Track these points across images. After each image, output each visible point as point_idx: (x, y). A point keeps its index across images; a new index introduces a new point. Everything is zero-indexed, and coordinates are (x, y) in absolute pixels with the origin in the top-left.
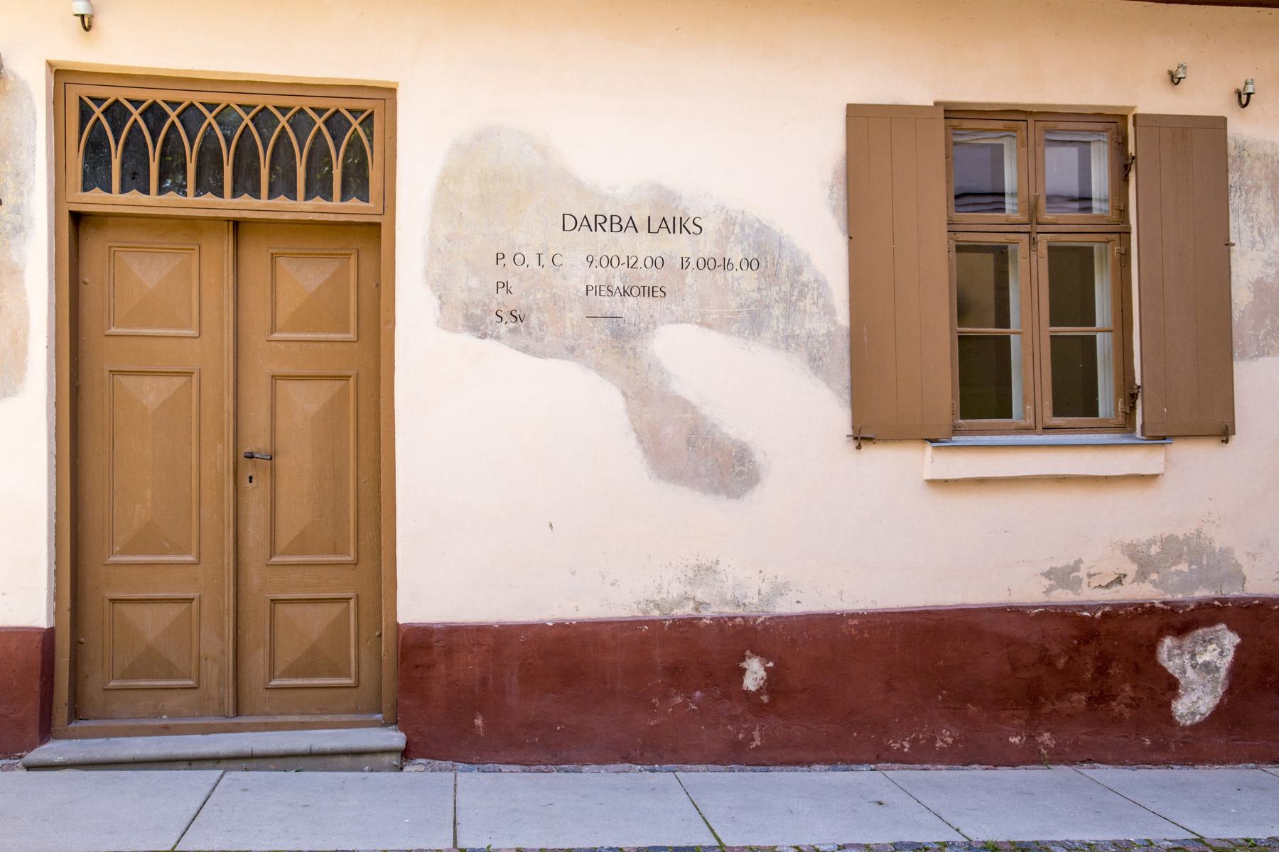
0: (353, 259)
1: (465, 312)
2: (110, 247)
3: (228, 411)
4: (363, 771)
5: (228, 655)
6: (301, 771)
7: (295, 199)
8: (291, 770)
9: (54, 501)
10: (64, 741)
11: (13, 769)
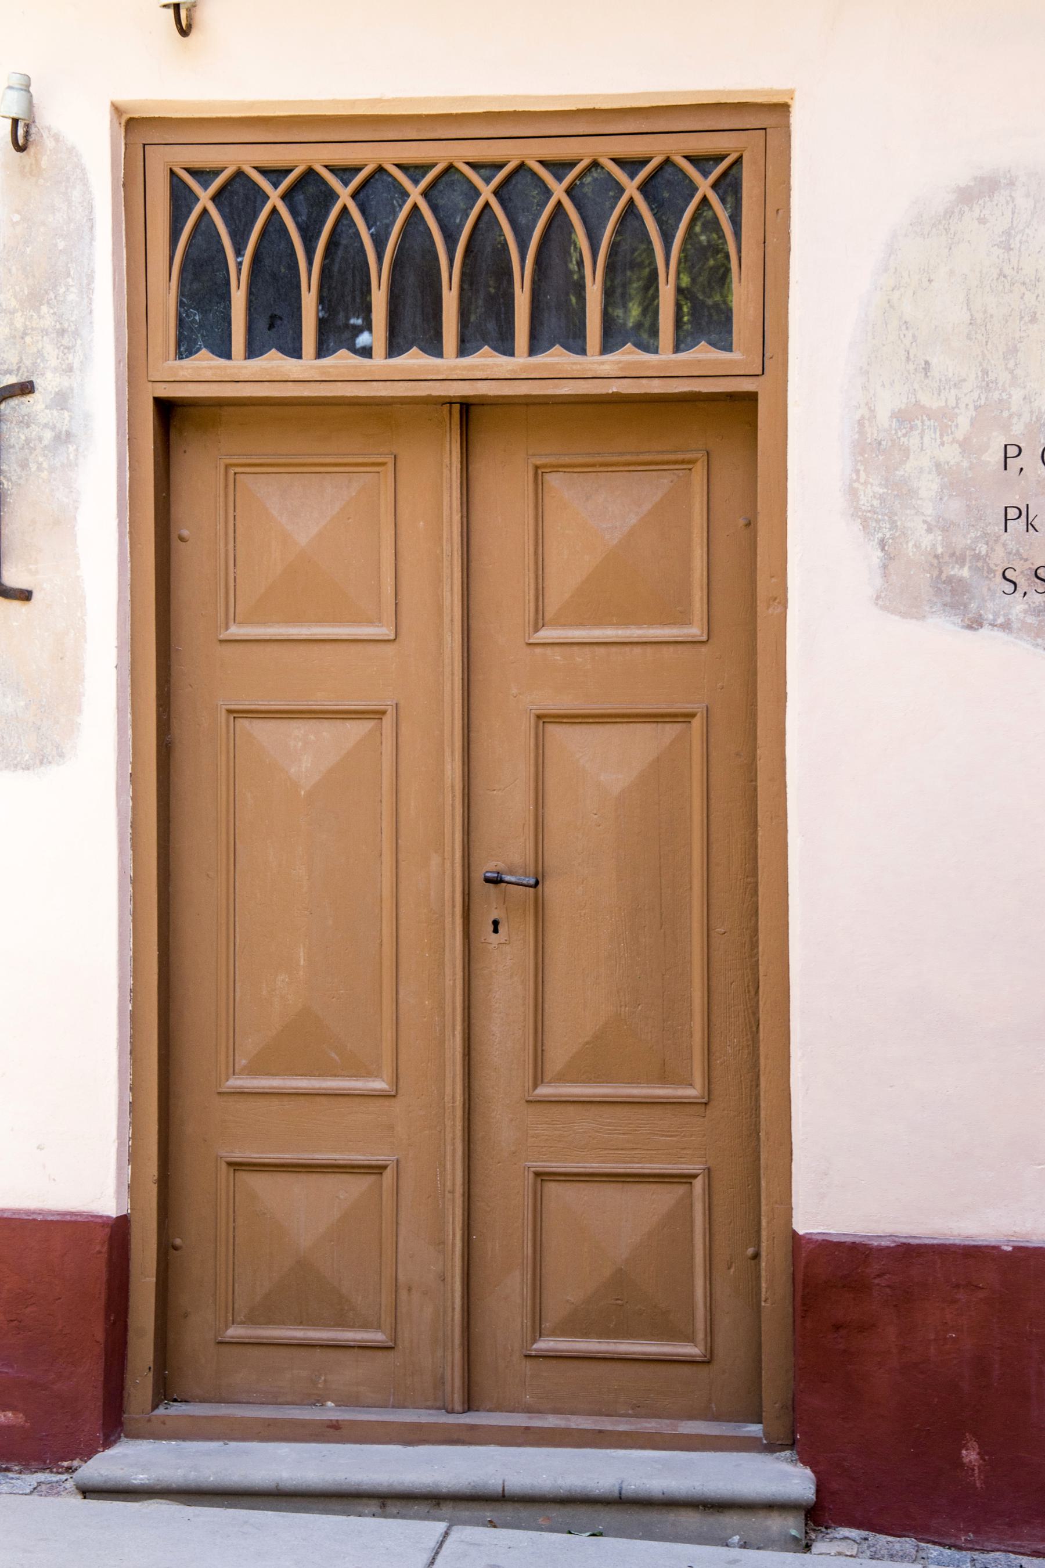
0: (698, 474)
1: (936, 573)
2: (227, 467)
3: (453, 787)
4: (727, 1545)
5: (453, 1283)
6: (601, 1535)
7: (583, 351)
8: (581, 1531)
9: (129, 968)
10: (145, 1442)
11: (58, 1494)
